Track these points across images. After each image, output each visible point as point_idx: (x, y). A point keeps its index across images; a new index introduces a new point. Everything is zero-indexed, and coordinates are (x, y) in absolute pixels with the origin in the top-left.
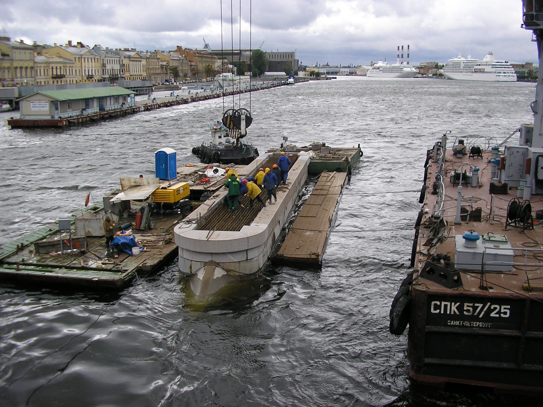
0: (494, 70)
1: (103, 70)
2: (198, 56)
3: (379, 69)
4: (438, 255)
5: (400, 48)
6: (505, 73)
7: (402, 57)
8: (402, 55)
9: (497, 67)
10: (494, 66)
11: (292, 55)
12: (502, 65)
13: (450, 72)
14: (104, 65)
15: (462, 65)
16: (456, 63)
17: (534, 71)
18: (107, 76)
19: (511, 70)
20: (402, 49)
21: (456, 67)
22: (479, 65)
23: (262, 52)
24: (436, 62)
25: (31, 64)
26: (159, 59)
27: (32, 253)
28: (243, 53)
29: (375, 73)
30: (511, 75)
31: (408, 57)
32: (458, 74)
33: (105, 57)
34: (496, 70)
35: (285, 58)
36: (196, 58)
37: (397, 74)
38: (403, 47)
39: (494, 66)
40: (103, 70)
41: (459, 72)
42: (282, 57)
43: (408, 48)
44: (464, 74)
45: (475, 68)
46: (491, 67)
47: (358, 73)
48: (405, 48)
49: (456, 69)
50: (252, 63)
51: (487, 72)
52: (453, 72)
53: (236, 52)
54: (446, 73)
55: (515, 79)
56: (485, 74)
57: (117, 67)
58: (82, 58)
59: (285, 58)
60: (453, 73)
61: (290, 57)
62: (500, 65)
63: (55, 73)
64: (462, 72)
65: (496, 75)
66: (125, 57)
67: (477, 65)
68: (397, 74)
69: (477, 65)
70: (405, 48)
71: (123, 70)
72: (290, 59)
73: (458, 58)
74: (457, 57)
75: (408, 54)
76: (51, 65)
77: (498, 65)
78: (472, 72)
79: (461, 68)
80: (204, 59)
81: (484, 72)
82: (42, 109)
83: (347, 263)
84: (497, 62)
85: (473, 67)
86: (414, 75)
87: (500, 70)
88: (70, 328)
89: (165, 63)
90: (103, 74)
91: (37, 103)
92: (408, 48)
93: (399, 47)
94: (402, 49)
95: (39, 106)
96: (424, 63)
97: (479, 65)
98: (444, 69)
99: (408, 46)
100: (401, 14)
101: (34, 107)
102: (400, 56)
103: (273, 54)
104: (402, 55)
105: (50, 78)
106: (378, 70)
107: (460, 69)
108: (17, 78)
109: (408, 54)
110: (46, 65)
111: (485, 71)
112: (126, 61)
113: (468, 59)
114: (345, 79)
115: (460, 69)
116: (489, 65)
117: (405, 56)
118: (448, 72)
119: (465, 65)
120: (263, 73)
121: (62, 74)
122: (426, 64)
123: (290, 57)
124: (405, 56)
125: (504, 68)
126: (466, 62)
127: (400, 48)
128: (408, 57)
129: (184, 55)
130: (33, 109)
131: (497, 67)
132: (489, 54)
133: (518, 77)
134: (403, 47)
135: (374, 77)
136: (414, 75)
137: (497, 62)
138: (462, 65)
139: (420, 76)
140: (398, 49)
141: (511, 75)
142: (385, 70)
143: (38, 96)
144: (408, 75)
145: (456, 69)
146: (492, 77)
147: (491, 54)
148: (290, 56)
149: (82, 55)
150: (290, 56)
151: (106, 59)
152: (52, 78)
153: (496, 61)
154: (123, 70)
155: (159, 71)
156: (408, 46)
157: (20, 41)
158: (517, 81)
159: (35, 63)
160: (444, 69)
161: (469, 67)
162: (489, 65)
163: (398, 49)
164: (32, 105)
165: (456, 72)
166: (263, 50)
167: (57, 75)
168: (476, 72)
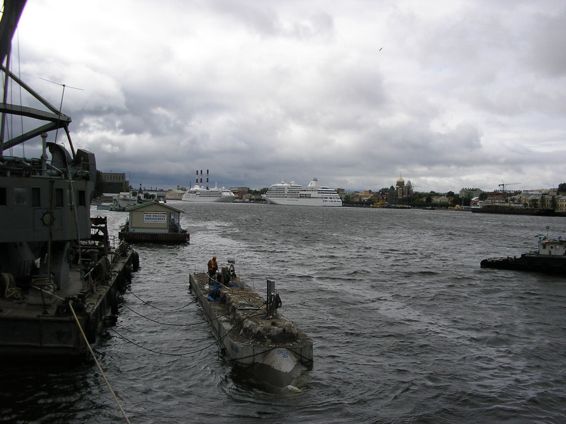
0: (320, 195)
3: (195, 193)
4: (110, 337)
5: (199, 172)
6: (331, 198)
7: (201, 182)
8: (201, 179)
9: (323, 193)
10: (321, 192)
11: (123, 176)
12: (328, 191)
13: (274, 197)
15: (286, 191)
16: (280, 188)
17: (351, 197)
19: (337, 196)
20: (201, 173)
21: (280, 192)
22: (305, 191)
23: (99, 171)
27: (203, 315)
29: (191, 197)
30: (336, 200)
31: (208, 182)
34: (322, 195)
35: (115, 179)
38: (201, 171)
39: (319, 192)
41: (284, 197)
42: (110, 178)
43: (208, 173)
44: (289, 199)
45: (300, 193)
46: (317, 192)
47: (167, 196)
48: (205, 172)
49: (280, 194)
51: (313, 198)
52: (276, 197)
55: (341, 204)
56: (311, 199)
59: (115, 179)
60: (277, 199)
61: (121, 179)
62: (326, 191)
64: (286, 197)
65: (323, 200)
67: (303, 190)
69: (303, 190)
70: (205, 172)
72: (121, 181)
73: (282, 184)
74: (280, 182)
75: (208, 179)
77: (324, 191)
78: (298, 198)
81: (310, 197)
84: (323, 188)
85: (299, 193)
87: (326, 196)
91: (152, 215)
92: (208, 173)
93: (197, 171)
94: (201, 173)
96: (236, 187)
97: (305, 191)
99: (208, 170)
100: (156, 132)
101: (148, 219)
102: (199, 181)
104: (201, 179)
107: (284, 195)
109: (208, 179)
111: (311, 196)
113: (292, 185)
115: (284, 195)
116: (315, 190)
117: (204, 180)
118: (271, 197)
119: (289, 190)
120: (101, 194)
122: (237, 189)
124: (204, 180)
125: (330, 193)
126: (290, 187)
127: (199, 172)
128: (208, 182)
130: (146, 221)
131: (323, 193)
132: (314, 180)
133: (343, 202)
134: (201, 171)
137: (323, 188)
138: (286, 191)
140: (197, 174)
141: (336, 200)
142: (202, 194)
144: (227, 199)
145: (280, 194)
146: (319, 203)
147: (315, 180)
148: (121, 177)
150: (121, 177)
153: (322, 187)
156: (208, 170)
158: (343, 206)
160: (267, 194)
161: (293, 193)
162: (315, 190)
163: (197, 174)
164: (145, 217)
165: (280, 197)
168: (301, 197)
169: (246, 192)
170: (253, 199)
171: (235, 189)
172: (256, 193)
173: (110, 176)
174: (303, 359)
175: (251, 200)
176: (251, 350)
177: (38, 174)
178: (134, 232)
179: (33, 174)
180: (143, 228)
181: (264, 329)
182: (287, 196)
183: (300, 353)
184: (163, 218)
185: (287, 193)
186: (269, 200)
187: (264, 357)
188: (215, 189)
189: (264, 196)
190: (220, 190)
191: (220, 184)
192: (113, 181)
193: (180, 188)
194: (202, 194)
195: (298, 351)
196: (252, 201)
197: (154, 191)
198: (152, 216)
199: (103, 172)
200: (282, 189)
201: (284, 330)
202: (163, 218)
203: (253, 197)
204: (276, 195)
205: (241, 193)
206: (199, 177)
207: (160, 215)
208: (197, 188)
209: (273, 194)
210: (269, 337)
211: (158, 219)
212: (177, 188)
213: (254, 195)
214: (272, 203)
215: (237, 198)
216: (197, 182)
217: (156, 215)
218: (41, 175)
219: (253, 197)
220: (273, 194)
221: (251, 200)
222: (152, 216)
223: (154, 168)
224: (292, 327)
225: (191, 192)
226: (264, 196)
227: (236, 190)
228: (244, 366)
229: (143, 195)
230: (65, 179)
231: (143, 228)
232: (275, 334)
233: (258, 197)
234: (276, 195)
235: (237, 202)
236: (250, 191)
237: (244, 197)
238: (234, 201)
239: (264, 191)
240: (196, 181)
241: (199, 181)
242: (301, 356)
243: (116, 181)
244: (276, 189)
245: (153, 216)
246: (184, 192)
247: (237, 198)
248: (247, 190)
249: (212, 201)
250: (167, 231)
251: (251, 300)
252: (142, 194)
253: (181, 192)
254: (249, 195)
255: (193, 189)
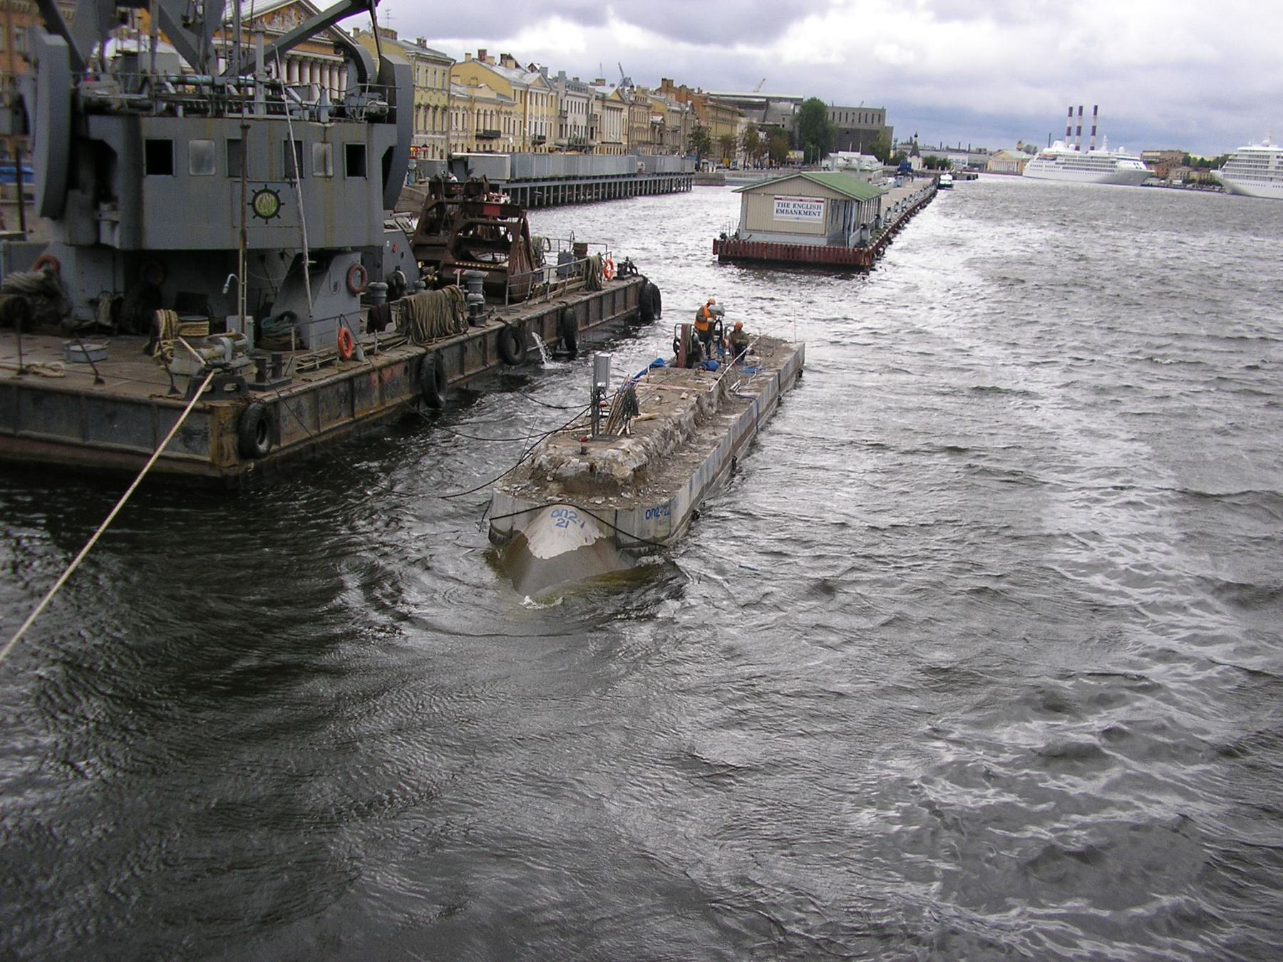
1: (561, 126)
2: (712, 106)
3: (1054, 159)
5: (1076, 111)
7: (1079, 133)
8: (1079, 128)
11: (880, 114)
13: (1240, 177)
14: (563, 115)
16: (1258, 156)
18: (565, 142)
24: (1184, 150)
25: (443, 101)
26: (649, 107)
28: (771, 104)
29: (1044, 168)
31: (1094, 134)
32: (1262, 182)
33: (566, 95)
36: (708, 109)
37: (1103, 175)
38: (1081, 108)
40: (561, 126)
41: (1265, 179)
43: (1095, 113)
47: (991, 165)
48: (1088, 110)
50: (797, 129)
53: (757, 100)
54: (1231, 181)
57: (582, 121)
58: (527, 92)
59: (843, 120)
60: (1249, 181)
61: (876, 121)
63: (481, 127)
66: (597, 98)
68: (1103, 175)
70: (1088, 110)
71: (592, 129)
72: (876, 126)
73: (1264, 145)
74: (1259, 141)
75: (1094, 128)
76: (477, 106)
79: (1272, 169)
80: (721, 115)
82: (805, 219)
83: (114, 285)
86: (1142, 180)
88: (1056, 719)
89: (658, 119)
90: (561, 136)
91: (792, 204)
92: (1095, 113)
93: (1071, 109)
95: (797, 209)
96: (1157, 148)
98: (1224, 170)
99: (1096, 108)
101: (782, 212)
102: (1074, 131)
103: (845, 112)
104: (1079, 128)
105: (471, 137)
106: (1053, 163)
108: (417, 132)
109: (1094, 128)
110: (468, 105)
112: (597, 108)
114: (995, 181)
117: (1086, 130)
118: (1234, 177)
121: (494, 129)
122: (1158, 154)
123: (876, 121)
124: (1086, 130)
127: (1076, 111)
128: (1094, 134)
129: (689, 102)
130: (778, 217)
134: (1081, 108)
135: (1037, 174)
136: (1142, 180)
138: (1274, 163)
139: (1154, 181)
140: (1070, 115)
142: (1070, 164)
143: (798, 181)
148: (876, 117)
149: (528, 86)
150: (876, 117)
151: (567, 98)
152: (478, 137)
154: (592, 129)
155: (647, 137)
156: (1096, 108)
157: (416, 42)
159: (450, 97)
160: (1224, 170)
163: (1070, 115)
164: (776, 205)
165: (1256, 178)
166: (827, 101)
167: (485, 131)
169: (1178, 163)
170: (1193, 181)
171: (1154, 154)
172: (1204, 165)
173: (863, 115)
174: (621, 536)
175: (1187, 181)
176: (510, 503)
177: (246, 110)
178: (751, 240)
179: (229, 111)
180: (771, 232)
181: (550, 461)
182: (1272, 176)
183: (612, 523)
184: (815, 211)
185: (1273, 169)
186: (1227, 183)
187: (531, 520)
188: (1101, 152)
189: (1217, 174)
190: (1113, 154)
191: (1115, 141)
192: (866, 127)
193: (1025, 146)
194: (1070, 164)
195: (608, 517)
196: (1190, 186)
197: (964, 151)
198: (791, 206)
199: (829, 104)
200: (1262, 159)
201: (592, 468)
202: (815, 211)
203: (1195, 175)
204: (1248, 171)
205: (1165, 164)
206: (1074, 122)
207: (809, 204)
208: (1059, 147)
209: (1240, 171)
210: (557, 479)
211: (805, 213)
212: (1015, 146)
213: (1196, 170)
214: (1236, 193)
215: (1152, 176)
216: (1069, 134)
217: (800, 203)
218: (251, 112)
219: (1195, 175)
220: (1240, 171)
221: (1187, 181)
222: (791, 206)
223: (987, 101)
224: (618, 463)
225: (1044, 158)
226: (1217, 174)
227: (1156, 157)
228: (498, 535)
229: (920, 160)
230: (310, 120)
231: (771, 232)
232: (571, 473)
233: (1204, 176)
234: (1248, 171)
235: (1152, 186)
236: (1187, 161)
237: (1173, 173)
238: (1146, 182)
239: (1219, 163)
240: (1066, 132)
241: (1074, 131)
242: (614, 528)
243: (862, 126)
244: (1246, 158)
245: (794, 206)
246: (1029, 156)
247: (1152, 176)
248: (1181, 158)
249: (1093, 179)
250: (822, 242)
251: (658, 399)
252: (919, 156)
253: (1025, 156)
254: (1186, 169)
255: (1050, 150)
